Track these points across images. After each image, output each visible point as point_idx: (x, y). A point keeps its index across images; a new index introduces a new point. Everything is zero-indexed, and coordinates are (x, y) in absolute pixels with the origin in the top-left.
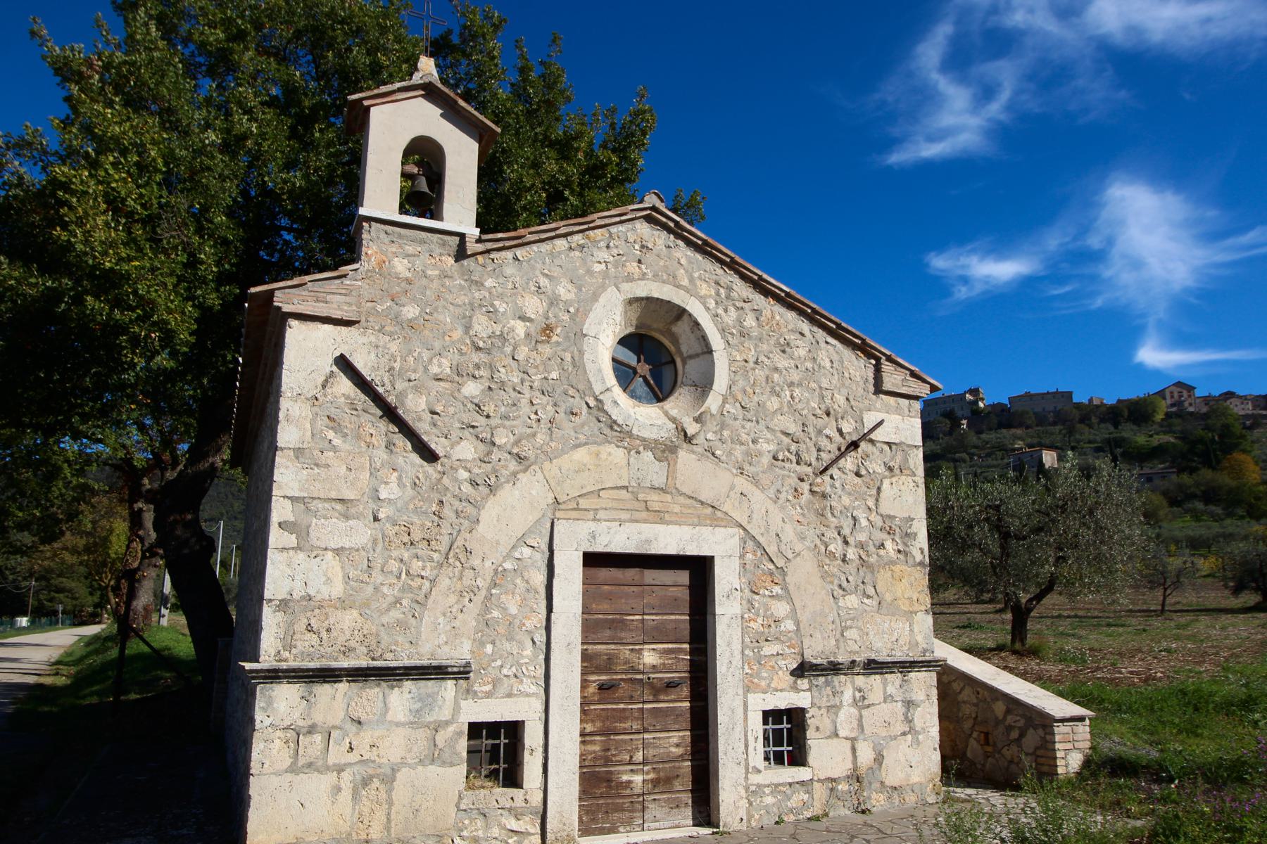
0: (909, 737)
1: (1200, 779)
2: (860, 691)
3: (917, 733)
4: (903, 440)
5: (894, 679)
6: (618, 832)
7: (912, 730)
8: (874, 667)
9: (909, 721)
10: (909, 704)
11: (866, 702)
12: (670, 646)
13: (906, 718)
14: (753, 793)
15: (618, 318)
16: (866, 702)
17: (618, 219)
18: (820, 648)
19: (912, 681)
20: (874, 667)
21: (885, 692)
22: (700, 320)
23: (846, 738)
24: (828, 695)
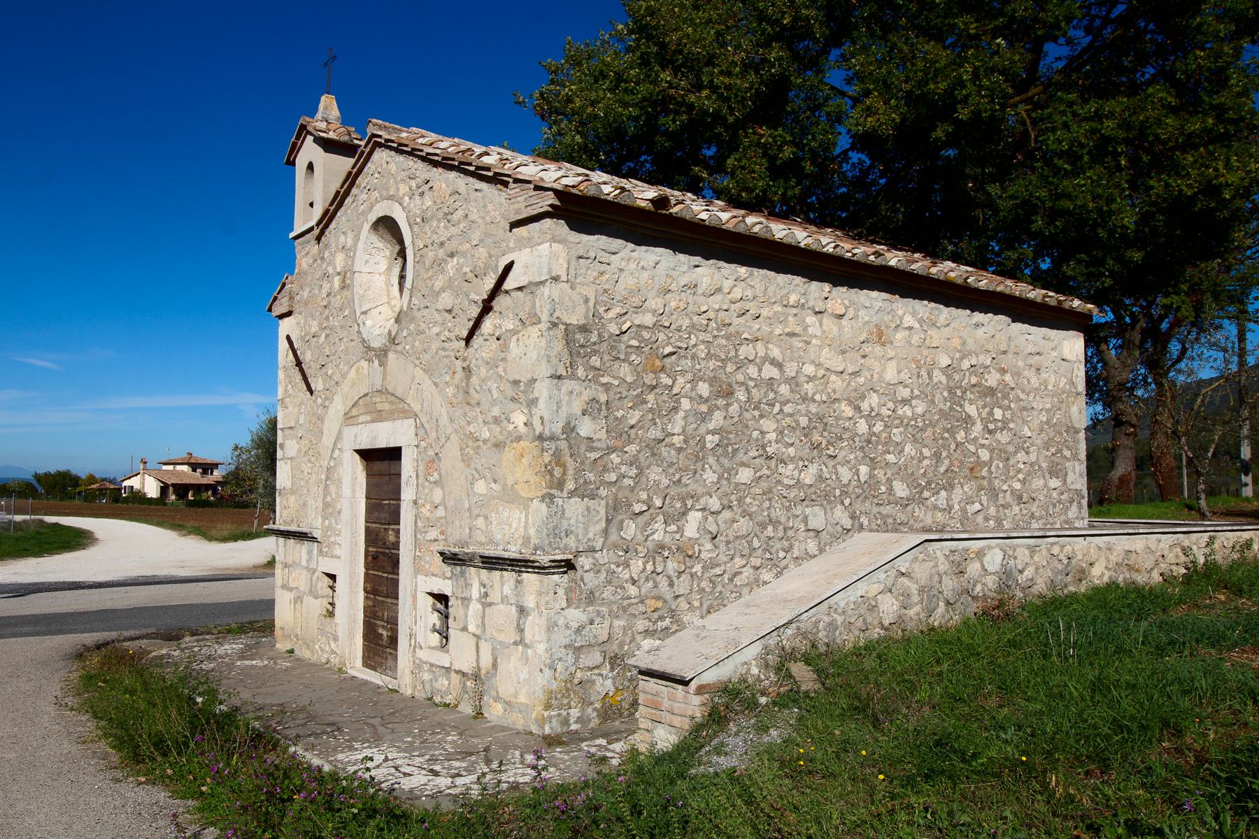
0: (520, 647)
2: (484, 586)
4: (531, 279)
7: (521, 642)
9: (521, 630)
10: (522, 611)
11: (489, 600)
13: (518, 625)
14: (418, 666)
16: (489, 600)
17: (1213, 528)
18: (458, 537)
19: (525, 581)
23: (474, 635)
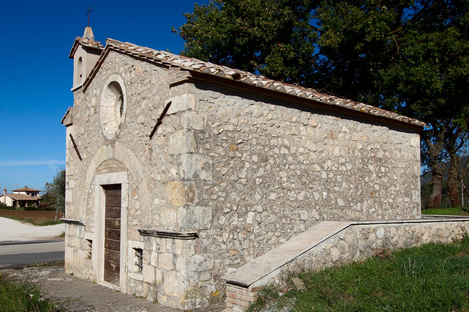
0: (174, 272)
1: (416, 208)
2: (158, 245)
3: (177, 271)
5: (169, 241)
6: (110, 283)
7: (174, 269)
8: (162, 235)
9: (175, 264)
10: (175, 256)
11: (160, 251)
12: (158, 62)
15: (112, 94)
18: (146, 224)
19: (176, 243)
20: (162, 235)
21: (166, 248)
22: (49, 227)
23: (154, 266)
24: (148, 245)
